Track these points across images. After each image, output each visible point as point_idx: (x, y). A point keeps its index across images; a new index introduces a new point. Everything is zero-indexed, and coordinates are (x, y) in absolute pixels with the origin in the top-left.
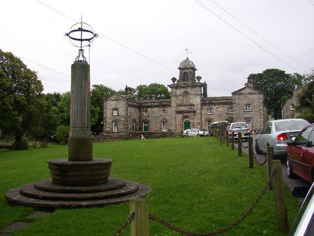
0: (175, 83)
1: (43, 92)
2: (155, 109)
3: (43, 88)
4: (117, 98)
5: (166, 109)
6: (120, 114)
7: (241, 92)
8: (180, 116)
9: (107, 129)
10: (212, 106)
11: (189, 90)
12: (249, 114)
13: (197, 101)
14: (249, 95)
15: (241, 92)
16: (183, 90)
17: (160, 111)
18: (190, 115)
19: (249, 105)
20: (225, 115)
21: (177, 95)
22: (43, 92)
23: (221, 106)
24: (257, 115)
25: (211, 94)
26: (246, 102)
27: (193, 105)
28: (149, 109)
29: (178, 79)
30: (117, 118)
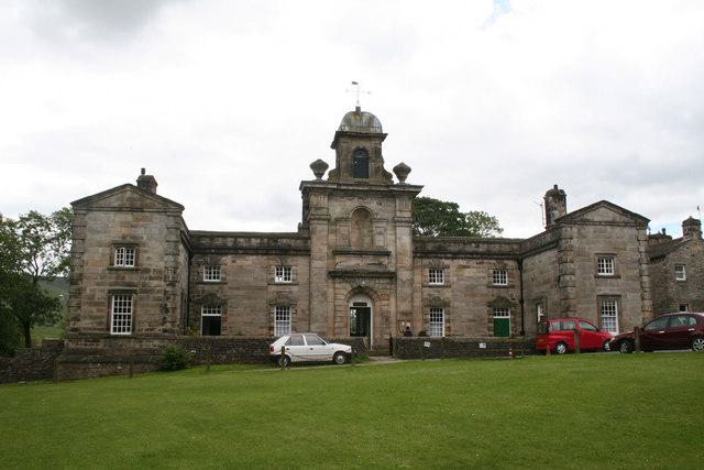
0: (325, 177)
2: (250, 261)
4: (138, 204)
5: (290, 261)
6: (145, 263)
7: (585, 217)
8: (344, 288)
10: (446, 262)
11: (373, 205)
12: (611, 285)
13: (399, 240)
14: (609, 228)
15: (585, 217)
17: (267, 268)
18: (378, 285)
19: (609, 257)
20: (484, 290)
21: (333, 220)
23: (473, 263)
24: (635, 291)
26: (600, 247)
27: (387, 254)
28: (227, 259)
29: (332, 166)
30: (135, 278)
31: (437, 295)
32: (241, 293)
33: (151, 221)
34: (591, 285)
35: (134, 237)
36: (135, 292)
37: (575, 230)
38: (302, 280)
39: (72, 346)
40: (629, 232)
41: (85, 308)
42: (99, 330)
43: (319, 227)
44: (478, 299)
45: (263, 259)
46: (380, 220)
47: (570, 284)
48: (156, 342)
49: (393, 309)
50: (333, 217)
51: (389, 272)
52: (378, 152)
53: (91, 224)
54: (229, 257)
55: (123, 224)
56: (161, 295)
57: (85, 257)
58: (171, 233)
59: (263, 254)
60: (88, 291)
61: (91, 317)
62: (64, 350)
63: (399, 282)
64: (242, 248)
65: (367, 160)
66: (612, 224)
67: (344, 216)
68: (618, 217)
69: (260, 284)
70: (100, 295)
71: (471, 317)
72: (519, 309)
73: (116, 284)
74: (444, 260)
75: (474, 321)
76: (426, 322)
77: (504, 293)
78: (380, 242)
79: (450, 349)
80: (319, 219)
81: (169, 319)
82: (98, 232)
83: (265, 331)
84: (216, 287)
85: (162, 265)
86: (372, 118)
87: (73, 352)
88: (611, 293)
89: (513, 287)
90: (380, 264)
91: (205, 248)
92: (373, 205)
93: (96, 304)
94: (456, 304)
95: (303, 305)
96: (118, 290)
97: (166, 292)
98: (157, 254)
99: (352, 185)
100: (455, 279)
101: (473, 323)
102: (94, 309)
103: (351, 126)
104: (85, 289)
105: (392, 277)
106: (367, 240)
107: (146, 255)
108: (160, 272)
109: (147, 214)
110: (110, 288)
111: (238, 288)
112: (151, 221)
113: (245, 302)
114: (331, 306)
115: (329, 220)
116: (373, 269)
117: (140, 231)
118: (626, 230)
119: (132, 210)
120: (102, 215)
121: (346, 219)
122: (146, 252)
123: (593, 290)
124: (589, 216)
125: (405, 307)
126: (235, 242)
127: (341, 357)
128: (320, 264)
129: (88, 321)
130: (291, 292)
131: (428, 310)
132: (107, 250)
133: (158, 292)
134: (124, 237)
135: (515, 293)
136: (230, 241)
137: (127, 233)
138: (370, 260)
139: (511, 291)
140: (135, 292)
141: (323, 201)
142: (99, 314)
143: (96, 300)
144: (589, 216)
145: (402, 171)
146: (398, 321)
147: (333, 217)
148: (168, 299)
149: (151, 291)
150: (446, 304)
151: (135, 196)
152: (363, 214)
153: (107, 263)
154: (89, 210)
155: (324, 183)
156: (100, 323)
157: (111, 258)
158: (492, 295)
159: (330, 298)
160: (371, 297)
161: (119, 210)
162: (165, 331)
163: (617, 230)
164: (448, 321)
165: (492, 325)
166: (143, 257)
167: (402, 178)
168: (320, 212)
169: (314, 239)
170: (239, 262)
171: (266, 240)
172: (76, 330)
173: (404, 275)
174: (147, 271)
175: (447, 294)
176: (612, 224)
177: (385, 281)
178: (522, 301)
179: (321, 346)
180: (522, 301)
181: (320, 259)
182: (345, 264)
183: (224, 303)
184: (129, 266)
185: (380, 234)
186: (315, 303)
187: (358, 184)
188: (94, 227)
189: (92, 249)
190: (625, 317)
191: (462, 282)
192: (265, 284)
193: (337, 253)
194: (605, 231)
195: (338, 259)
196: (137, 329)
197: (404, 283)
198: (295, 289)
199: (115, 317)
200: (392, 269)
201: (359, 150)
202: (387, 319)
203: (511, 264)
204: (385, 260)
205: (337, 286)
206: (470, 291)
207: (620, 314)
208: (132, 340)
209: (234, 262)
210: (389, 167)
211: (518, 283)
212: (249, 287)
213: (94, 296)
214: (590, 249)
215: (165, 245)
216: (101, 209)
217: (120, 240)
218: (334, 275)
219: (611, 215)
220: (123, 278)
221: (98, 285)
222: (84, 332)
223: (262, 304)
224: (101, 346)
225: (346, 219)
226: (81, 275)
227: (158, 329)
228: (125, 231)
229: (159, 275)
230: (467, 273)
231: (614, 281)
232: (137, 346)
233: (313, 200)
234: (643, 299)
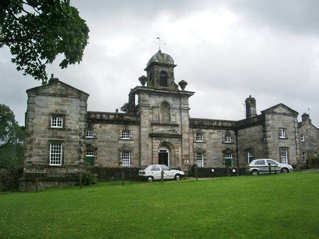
1: (146, 76)
3: (77, 63)
4: (64, 93)
5: (130, 128)
6: (68, 126)
8: (157, 143)
9: (35, 159)
10: (204, 130)
11: (170, 100)
14: (283, 116)
16: (160, 100)
18: (174, 141)
20: (220, 144)
21: (151, 107)
22: (146, 76)
23: (215, 131)
25: (93, 106)
26: (280, 125)
27: (177, 126)
28: (97, 126)
30: (63, 134)
31: (200, 147)
32: (104, 144)
33: (72, 102)
34: (277, 142)
35: (62, 111)
36: (63, 141)
37: (270, 116)
38: (136, 137)
39: (28, 171)
40: (291, 118)
41: (35, 150)
42: (43, 162)
43: (145, 111)
44: (218, 149)
45: (115, 126)
46: (174, 108)
47: (269, 142)
48: (76, 170)
49: (180, 154)
50: (151, 106)
51: (178, 135)
52: (172, 74)
53: (38, 102)
54: (98, 124)
55: (56, 104)
56: (78, 144)
57: (35, 121)
58: (82, 110)
59: (116, 124)
60: (37, 141)
61: (39, 156)
62: (24, 174)
63: (183, 140)
64: (105, 120)
65: (166, 77)
66: (284, 114)
67: (157, 105)
68: (286, 112)
69: (114, 139)
70: (43, 143)
71: (215, 158)
72: (236, 154)
73: (52, 137)
74: (202, 130)
75: (216, 160)
76: (195, 160)
77: (229, 146)
78: (173, 119)
79: (205, 173)
80: (145, 106)
81: (83, 157)
82: (42, 107)
83: (117, 164)
84: (91, 141)
85: (78, 127)
86: (168, 56)
87: (29, 175)
88: (284, 146)
89: (233, 143)
90: (174, 131)
91: (93, 119)
92: (170, 100)
93: (41, 148)
94: (209, 151)
95: (136, 151)
96: (54, 140)
97: (80, 142)
98: (75, 122)
99: (161, 90)
100: (208, 139)
101: (216, 161)
102: (40, 151)
103: (159, 60)
104: (35, 140)
105: (179, 137)
106: (167, 118)
107: (69, 121)
108: (77, 131)
109: (70, 99)
110: (49, 139)
111: (103, 142)
112: (72, 102)
113: (106, 149)
114: (150, 152)
115: (149, 107)
116: (171, 133)
117: (65, 108)
118: (289, 117)
119: (61, 96)
120: (44, 98)
121: (158, 107)
122: (69, 119)
123: (278, 145)
124: (275, 110)
125: (186, 152)
126: (101, 116)
127: (150, 178)
128: (145, 130)
129: (36, 158)
130: (130, 144)
131: (196, 154)
132: (47, 118)
133: (76, 142)
134: (57, 111)
135: (234, 146)
136: (98, 116)
137: (59, 108)
138: (169, 128)
139: (233, 145)
140: (63, 141)
141: (147, 97)
142: (43, 154)
143: (41, 146)
144: (275, 110)
145: (183, 84)
146: (183, 160)
147: (151, 106)
148: (82, 146)
149: (72, 141)
150: (204, 152)
151: (63, 88)
152: (165, 105)
153: (47, 125)
154: (37, 95)
155: (146, 88)
156: (44, 159)
157: (50, 122)
158: (224, 147)
159: (150, 148)
160: (169, 148)
161: (54, 95)
162: (80, 163)
163: (286, 117)
164: (205, 160)
165: (224, 162)
166: (68, 122)
167: (183, 88)
168: (145, 103)
169: (142, 117)
170: (103, 127)
171: (117, 116)
172: (30, 162)
173: (185, 136)
174: (70, 130)
175: (204, 147)
176: (284, 114)
177: (178, 139)
178: (237, 150)
179: (168, 171)
180: (237, 150)
181: (146, 127)
182: (157, 130)
183: (96, 149)
184: (59, 127)
185: (174, 115)
186: (143, 150)
187: (164, 89)
188: (39, 104)
189: (38, 117)
190: (290, 158)
191: (211, 141)
192: (117, 139)
193: (153, 124)
194: (282, 118)
195: (154, 127)
196: (65, 162)
197: (185, 140)
198: (132, 142)
199: (52, 155)
200: (179, 133)
201: (163, 72)
202: (178, 159)
203: (232, 132)
204: (176, 129)
205: (154, 141)
206: (215, 145)
207: (288, 156)
208: (63, 169)
209: (100, 127)
210: (177, 82)
211: (235, 142)
212: (108, 141)
213: (40, 143)
214: (276, 125)
215: (80, 116)
216: (44, 94)
217: (55, 112)
218: (152, 136)
219: (284, 110)
220: (57, 133)
221: (42, 137)
222: (34, 163)
223: (115, 150)
224: (45, 171)
225: (158, 107)
226: (33, 131)
227: (77, 162)
228: (57, 107)
229: (77, 133)
230: (214, 136)
231: (286, 141)
232: (65, 172)
233: (31, 105)
234: (296, 149)
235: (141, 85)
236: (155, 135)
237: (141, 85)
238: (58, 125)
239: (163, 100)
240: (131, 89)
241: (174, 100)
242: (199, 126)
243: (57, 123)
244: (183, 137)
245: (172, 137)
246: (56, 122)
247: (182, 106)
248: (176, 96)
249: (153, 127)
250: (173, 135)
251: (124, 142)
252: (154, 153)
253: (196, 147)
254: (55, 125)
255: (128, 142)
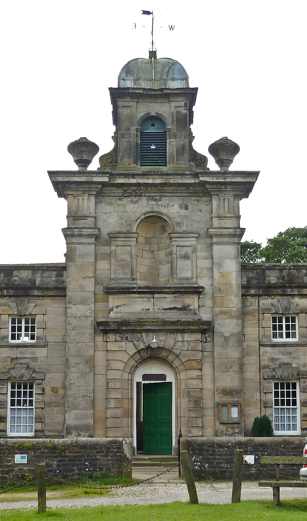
27: (198, 291)
31: (285, 359)
50: (105, 231)
51: (200, 322)
116: (173, 316)
121: (127, 234)
130: (34, 359)
138: (168, 301)
146: (219, 406)
147: (105, 231)
160: (164, 361)
167: (223, 162)
177: (199, 336)
181: (83, 302)
185: (186, 257)
195: (114, 301)
197: (226, 339)
198: (41, 353)
200: (205, 316)
205: (111, 346)
225: (127, 234)
235: (75, 168)
236: (113, 327)
237: (75, 168)
238: (288, 336)
239: (148, 209)
240: (112, 137)
241: (186, 208)
242: (283, 287)
243: (284, 331)
244: (217, 328)
245: (177, 331)
246: (281, 328)
247: (216, 222)
248: (194, 194)
249: (111, 298)
250: (178, 323)
251: (15, 353)
252: (111, 385)
253: (273, 360)
254: (281, 336)
255: (28, 353)
